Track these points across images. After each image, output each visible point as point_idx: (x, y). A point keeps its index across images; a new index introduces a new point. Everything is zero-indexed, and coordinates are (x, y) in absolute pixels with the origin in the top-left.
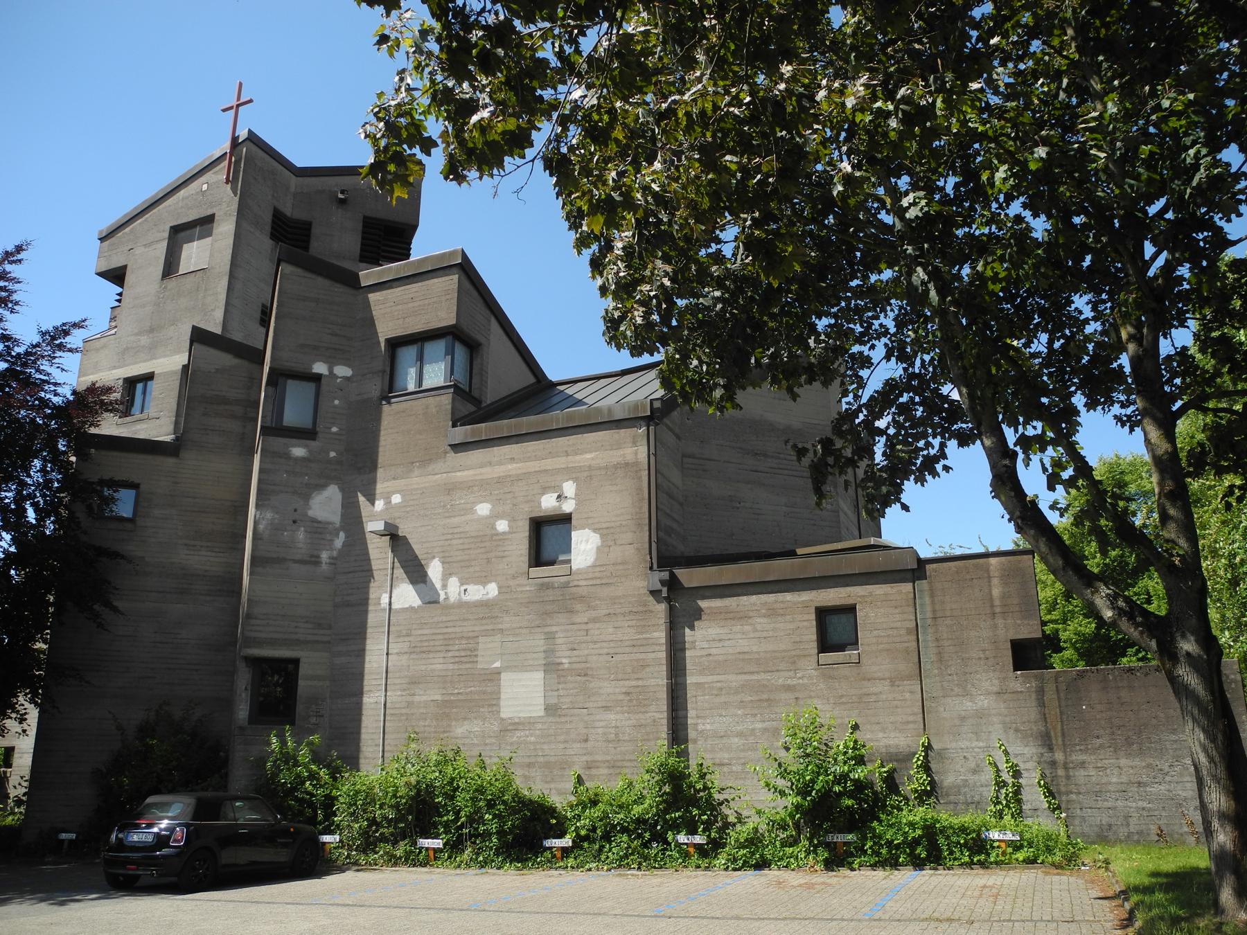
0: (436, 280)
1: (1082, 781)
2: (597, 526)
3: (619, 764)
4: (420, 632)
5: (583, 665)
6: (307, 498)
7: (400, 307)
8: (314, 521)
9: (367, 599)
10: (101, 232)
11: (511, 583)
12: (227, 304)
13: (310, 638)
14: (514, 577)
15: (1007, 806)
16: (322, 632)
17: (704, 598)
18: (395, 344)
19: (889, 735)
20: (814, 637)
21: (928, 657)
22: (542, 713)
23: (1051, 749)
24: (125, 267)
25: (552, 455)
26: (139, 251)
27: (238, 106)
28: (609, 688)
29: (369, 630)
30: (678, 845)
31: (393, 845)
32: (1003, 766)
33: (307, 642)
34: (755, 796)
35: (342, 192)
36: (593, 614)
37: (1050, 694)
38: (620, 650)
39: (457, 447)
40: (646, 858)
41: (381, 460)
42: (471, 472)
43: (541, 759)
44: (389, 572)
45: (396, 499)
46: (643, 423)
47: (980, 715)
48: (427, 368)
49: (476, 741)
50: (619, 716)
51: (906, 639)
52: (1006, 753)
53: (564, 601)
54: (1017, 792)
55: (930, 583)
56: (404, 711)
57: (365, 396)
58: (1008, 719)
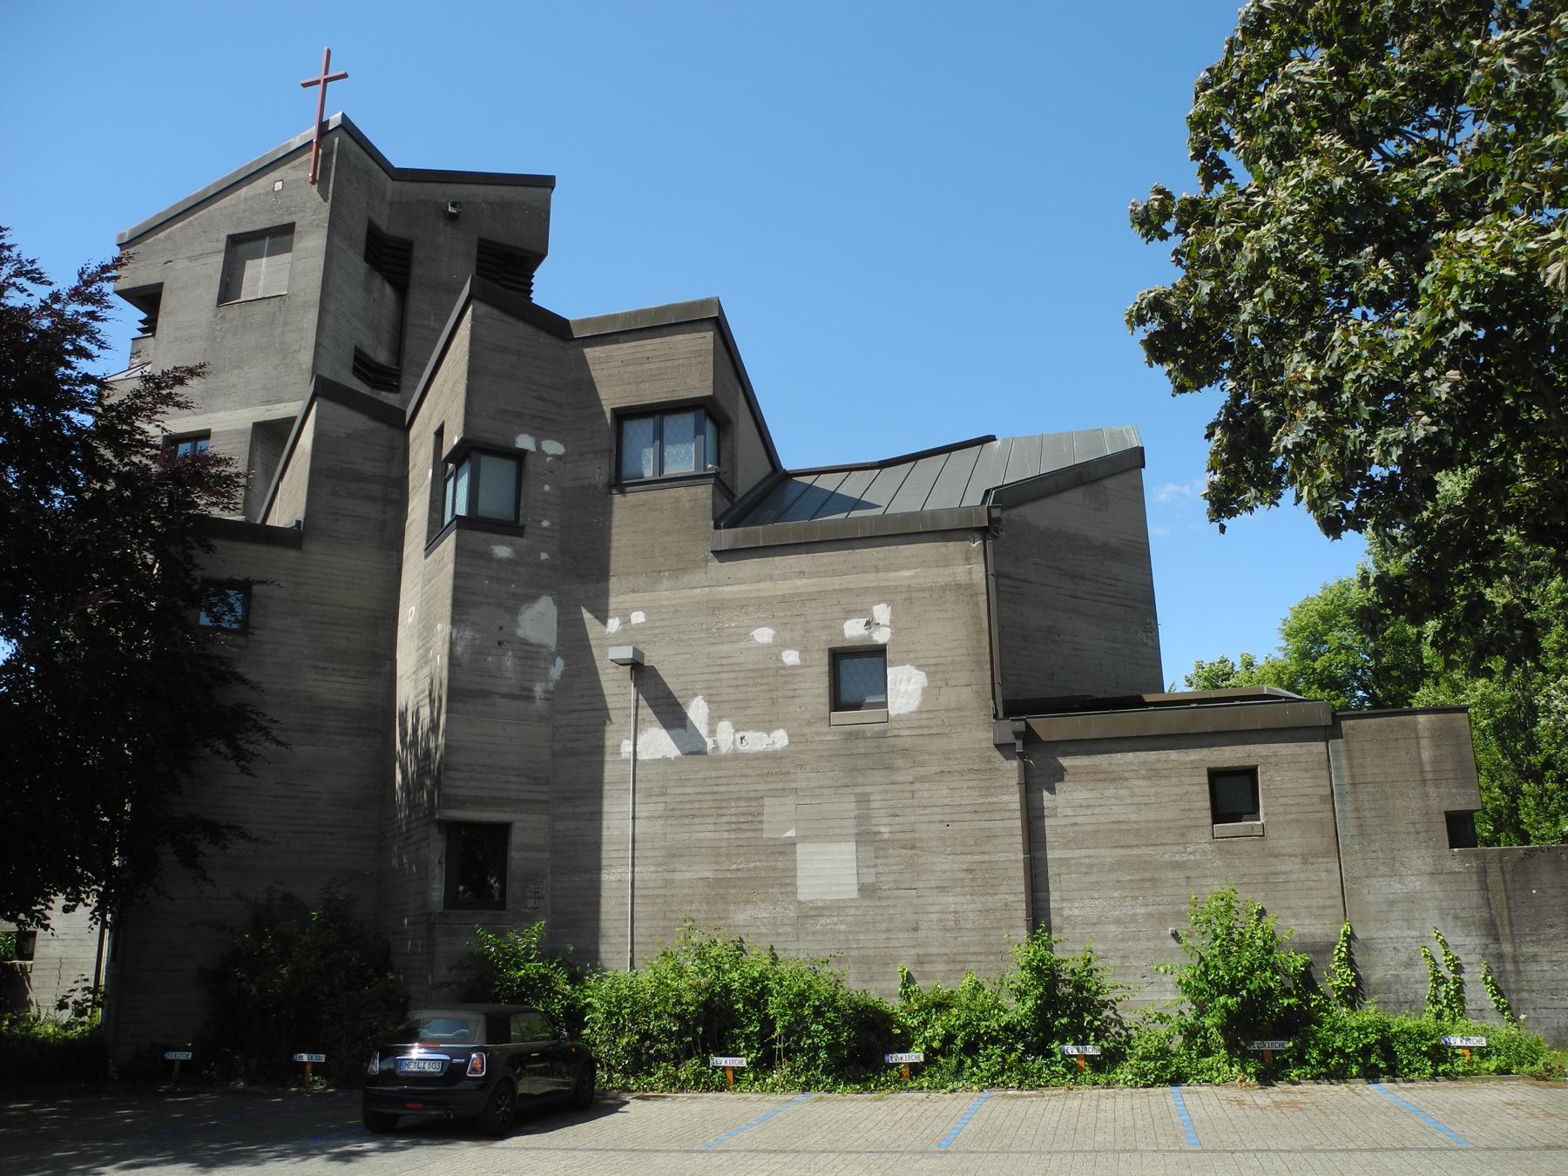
0: (681, 337)
1: (1534, 976)
2: (922, 662)
3: (961, 958)
4: (680, 790)
5: (908, 835)
6: (514, 612)
7: (630, 368)
8: (525, 643)
9: (603, 746)
10: (121, 236)
11: (806, 730)
12: (318, 344)
13: (525, 796)
14: (810, 723)
15: (1448, 1006)
16: (537, 788)
17: (1065, 754)
18: (624, 415)
19: (1300, 920)
20: (1208, 804)
21: (1347, 829)
22: (855, 895)
23: (1497, 940)
24: (161, 285)
25: (856, 570)
26: (181, 264)
27: (326, 81)
28: (943, 864)
29: (606, 787)
30: (1065, 1056)
31: (676, 1065)
32: (1441, 959)
33: (520, 802)
34: (1151, 994)
35: (454, 205)
36: (921, 771)
37: (1494, 877)
38: (957, 817)
39: (722, 555)
40: (1026, 1074)
41: (616, 564)
42: (744, 587)
43: (855, 953)
44: (633, 712)
45: (638, 618)
46: (977, 535)
47: (1412, 898)
48: (670, 451)
49: (763, 930)
50: (959, 899)
51: (1320, 807)
52: (1444, 944)
53: (883, 753)
54: (1459, 990)
55: (1347, 743)
56: (660, 892)
57: (586, 482)
58: (1444, 904)
